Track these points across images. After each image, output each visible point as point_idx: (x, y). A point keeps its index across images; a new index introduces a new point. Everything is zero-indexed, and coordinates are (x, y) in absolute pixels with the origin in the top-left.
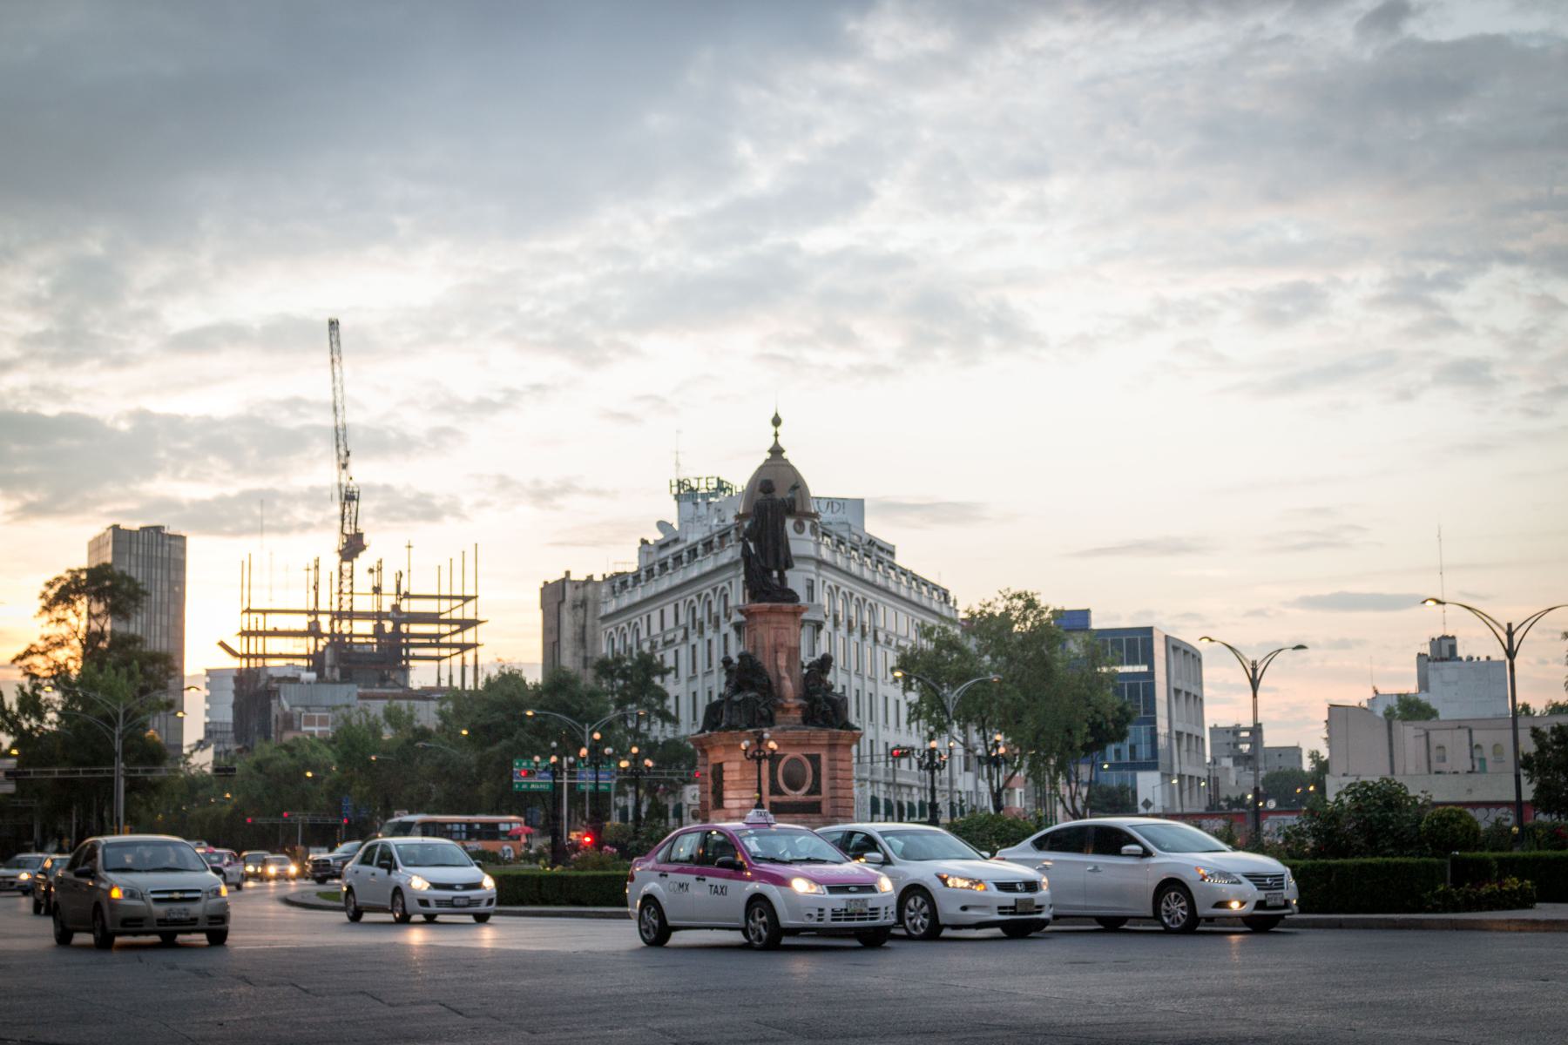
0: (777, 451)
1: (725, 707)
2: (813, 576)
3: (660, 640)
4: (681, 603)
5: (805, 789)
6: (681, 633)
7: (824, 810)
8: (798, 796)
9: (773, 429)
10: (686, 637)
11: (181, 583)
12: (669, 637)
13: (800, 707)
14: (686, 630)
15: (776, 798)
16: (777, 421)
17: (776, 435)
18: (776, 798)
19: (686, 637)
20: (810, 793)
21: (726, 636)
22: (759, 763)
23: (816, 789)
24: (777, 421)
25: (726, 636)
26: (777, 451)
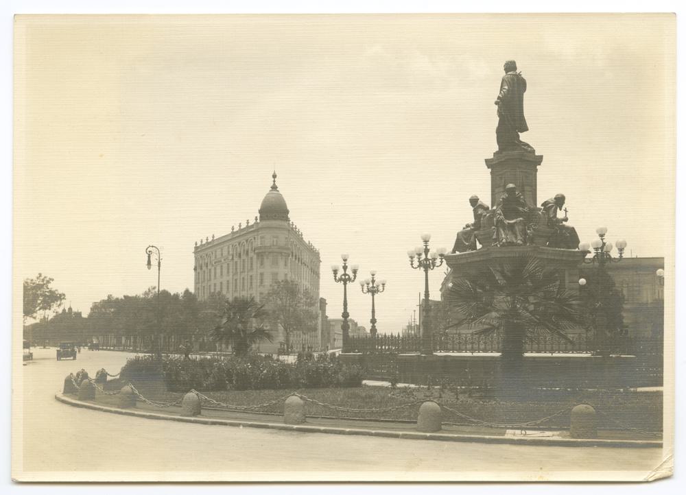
0: (274, 188)
6: (231, 258)
10: (233, 259)
14: (233, 256)
16: (274, 176)
17: (274, 181)
19: (233, 259)
24: (274, 176)
25: (252, 258)
26: (274, 188)
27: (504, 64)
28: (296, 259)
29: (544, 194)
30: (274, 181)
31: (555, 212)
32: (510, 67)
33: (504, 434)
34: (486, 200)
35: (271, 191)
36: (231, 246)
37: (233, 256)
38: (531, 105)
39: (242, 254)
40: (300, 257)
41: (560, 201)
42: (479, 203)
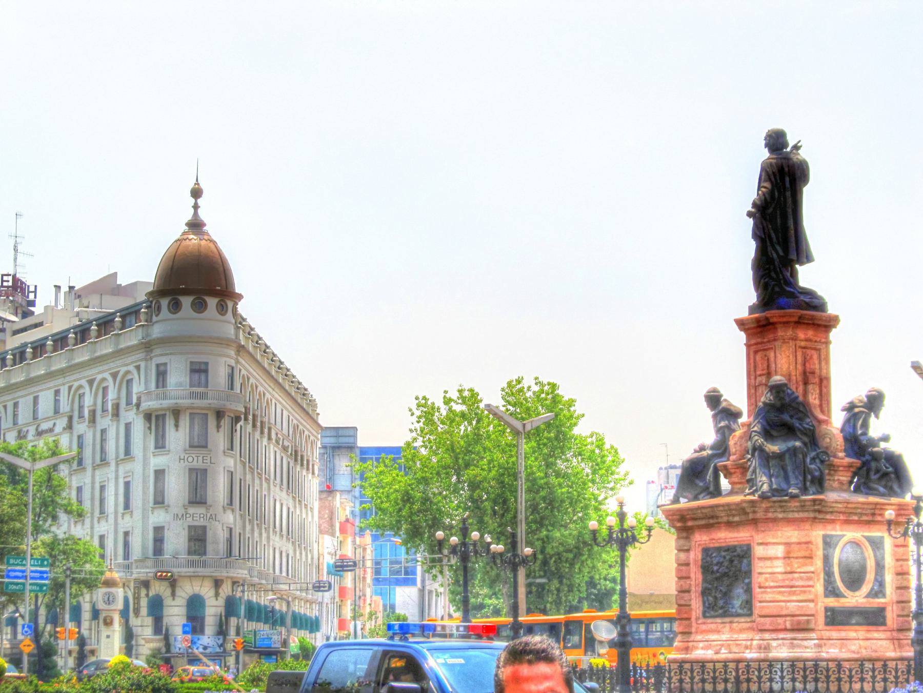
0: (196, 225)
1: (787, 456)
2: (233, 363)
3: (32, 430)
4: (64, 391)
5: (865, 589)
6: (62, 423)
7: (889, 621)
8: (856, 599)
9: (193, 200)
10: (70, 427)
11: (101, 280)
12: (45, 426)
13: (850, 466)
14: (70, 418)
15: (832, 602)
16: (196, 193)
17: (196, 207)
18: (832, 602)
19: (70, 427)
20: (873, 594)
21: (128, 426)
22: (515, 570)
23: (878, 591)
24: (196, 193)
25: (128, 426)
26: (196, 225)
27: (764, 135)
28: (254, 426)
29: (844, 388)
30: (196, 207)
31: (865, 425)
32: (776, 141)
33: (71, 620)
34: (737, 396)
35: (184, 233)
36: (64, 391)
37: (70, 418)
38: (819, 212)
39: (99, 412)
40: (258, 413)
41: (874, 402)
42: (724, 404)
